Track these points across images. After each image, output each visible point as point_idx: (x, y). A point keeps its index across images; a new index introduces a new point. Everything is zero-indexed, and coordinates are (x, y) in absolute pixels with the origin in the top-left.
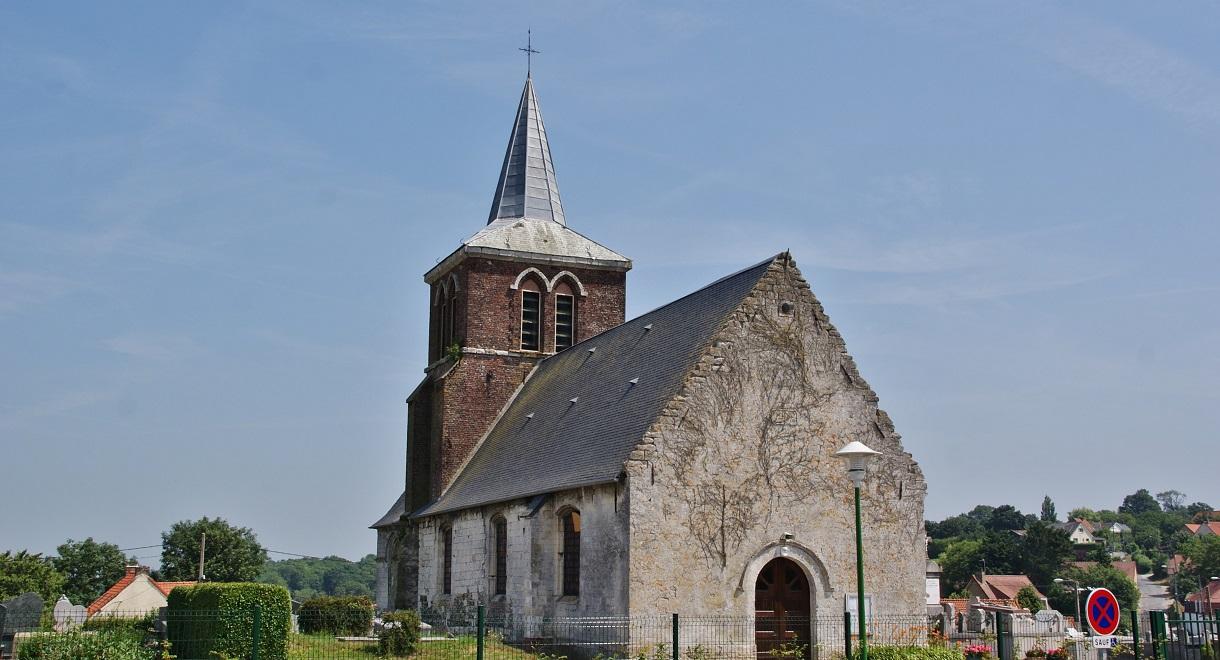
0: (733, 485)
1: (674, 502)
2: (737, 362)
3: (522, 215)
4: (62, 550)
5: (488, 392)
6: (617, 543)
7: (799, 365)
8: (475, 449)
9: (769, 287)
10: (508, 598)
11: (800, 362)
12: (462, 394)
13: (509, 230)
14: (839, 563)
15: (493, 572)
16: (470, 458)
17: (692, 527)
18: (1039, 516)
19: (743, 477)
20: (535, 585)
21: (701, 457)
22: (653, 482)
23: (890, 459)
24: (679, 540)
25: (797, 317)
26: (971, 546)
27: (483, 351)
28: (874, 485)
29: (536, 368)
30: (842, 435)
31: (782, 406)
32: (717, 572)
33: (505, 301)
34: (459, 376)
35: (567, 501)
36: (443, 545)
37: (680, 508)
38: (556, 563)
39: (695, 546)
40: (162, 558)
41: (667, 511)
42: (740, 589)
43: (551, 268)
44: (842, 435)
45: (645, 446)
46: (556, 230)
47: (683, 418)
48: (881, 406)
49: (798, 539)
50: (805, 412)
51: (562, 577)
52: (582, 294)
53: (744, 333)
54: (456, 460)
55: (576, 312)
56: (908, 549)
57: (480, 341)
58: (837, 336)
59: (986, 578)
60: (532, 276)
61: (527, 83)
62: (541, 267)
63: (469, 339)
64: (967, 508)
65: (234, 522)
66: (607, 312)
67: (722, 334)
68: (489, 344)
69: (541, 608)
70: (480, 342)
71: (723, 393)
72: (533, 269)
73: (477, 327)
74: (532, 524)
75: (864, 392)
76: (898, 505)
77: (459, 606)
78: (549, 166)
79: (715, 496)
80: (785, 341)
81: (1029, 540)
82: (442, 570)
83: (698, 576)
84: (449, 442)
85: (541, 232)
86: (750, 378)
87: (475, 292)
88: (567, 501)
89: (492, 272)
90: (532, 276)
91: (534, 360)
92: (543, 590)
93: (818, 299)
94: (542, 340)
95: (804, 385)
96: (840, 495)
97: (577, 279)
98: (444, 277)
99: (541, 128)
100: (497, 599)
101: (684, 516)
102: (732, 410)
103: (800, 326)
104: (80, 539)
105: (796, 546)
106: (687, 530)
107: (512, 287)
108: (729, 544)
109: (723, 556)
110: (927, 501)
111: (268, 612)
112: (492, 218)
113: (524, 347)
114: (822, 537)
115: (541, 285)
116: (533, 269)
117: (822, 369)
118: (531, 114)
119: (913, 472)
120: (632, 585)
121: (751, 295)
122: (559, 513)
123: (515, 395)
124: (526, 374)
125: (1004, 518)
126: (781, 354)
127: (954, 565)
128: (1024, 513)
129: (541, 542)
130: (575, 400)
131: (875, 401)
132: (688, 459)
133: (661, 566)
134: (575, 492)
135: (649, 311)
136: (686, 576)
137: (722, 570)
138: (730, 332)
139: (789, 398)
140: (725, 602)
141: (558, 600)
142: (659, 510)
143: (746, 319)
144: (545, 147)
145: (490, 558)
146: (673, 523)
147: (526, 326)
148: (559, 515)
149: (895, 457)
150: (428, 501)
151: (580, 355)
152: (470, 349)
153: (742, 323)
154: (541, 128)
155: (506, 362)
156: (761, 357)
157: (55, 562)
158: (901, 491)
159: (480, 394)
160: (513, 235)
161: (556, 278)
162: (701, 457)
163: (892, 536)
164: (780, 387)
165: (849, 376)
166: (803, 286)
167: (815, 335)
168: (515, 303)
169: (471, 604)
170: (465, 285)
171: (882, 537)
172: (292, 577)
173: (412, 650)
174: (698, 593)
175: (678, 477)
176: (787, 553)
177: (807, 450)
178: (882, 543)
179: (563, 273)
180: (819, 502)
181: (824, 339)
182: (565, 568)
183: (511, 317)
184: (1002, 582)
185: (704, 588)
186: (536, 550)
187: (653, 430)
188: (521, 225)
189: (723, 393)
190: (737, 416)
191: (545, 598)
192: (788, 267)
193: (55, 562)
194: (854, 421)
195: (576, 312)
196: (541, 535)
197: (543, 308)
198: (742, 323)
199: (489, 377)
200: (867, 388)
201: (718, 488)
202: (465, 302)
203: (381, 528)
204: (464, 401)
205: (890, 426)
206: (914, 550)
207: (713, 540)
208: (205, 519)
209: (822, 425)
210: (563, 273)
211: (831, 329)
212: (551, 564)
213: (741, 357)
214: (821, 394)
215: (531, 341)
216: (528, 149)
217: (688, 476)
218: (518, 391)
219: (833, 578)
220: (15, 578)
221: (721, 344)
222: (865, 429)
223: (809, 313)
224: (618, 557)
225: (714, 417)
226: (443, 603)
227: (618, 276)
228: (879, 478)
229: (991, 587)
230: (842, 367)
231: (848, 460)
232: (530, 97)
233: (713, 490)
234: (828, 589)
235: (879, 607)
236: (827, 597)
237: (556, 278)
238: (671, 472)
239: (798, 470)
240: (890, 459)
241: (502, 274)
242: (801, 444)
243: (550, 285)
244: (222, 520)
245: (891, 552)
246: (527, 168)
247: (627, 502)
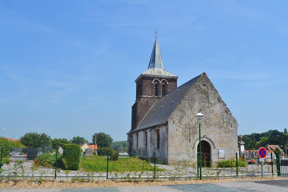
0: (192, 124)
1: (178, 128)
2: (193, 97)
3: (154, 67)
4: (74, 138)
5: (147, 105)
6: (166, 137)
8: (144, 117)
9: (200, 80)
10: (147, 149)
11: (208, 97)
13: (152, 71)
14: (217, 142)
15: (145, 143)
16: (143, 119)
17: (183, 134)
18: (283, 132)
19: (194, 122)
20: (151, 146)
21: (185, 118)
22: (174, 124)
23: (229, 118)
24: (180, 136)
26: (267, 139)
27: (146, 96)
28: (225, 124)
29: (157, 100)
30: (218, 113)
31: (204, 107)
32: (188, 143)
33: (150, 86)
34: (141, 102)
35: (157, 128)
36: (137, 137)
37: (180, 129)
38: (156, 141)
39: (183, 138)
40: (92, 140)
41: (177, 130)
42: (194, 147)
43: (160, 78)
44: (218, 113)
45: (172, 116)
46: (162, 70)
47: (181, 110)
49: (207, 136)
50: (209, 108)
51: (157, 145)
52: (167, 84)
53: (195, 91)
55: (166, 88)
56: (234, 139)
57: (145, 94)
58: (217, 91)
59: (269, 146)
60: (156, 80)
61: (156, 39)
62: (158, 78)
64: (267, 131)
65: (106, 133)
67: (189, 91)
68: (147, 95)
69: (152, 151)
71: (190, 104)
72: (156, 79)
73: (145, 91)
74: (151, 133)
75: (223, 103)
76: (231, 129)
77: (140, 151)
78: (160, 57)
79: (188, 127)
80: (204, 92)
81: (280, 137)
82: (137, 143)
83: (184, 144)
84: (139, 116)
85: (161, 71)
86: (196, 101)
88: (157, 128)
89: (148, 80)
90: (156, 80)
91: (157, 98)
92: (153, 147)
93: (212, 83)
94: (159, 94)
95: (209, 102)
96: (218, 127)
97: (166, 81)
98: (139, 81)
99: (159, 49)
100: (146, 149)
101: (181, 131)
102: (192, 108)
103: (208, 89)
104: (77, 136)
105: (207, 138)
106: (181, 134)
107: (152, 83)
109: (190, 140)
110: (238, 128)
111: (75, 151)
112: (148, 68)
113: (155, 95)
114: (212, 135)
116: (156, 79)
117: (213, 98)
118: (156, 46)
120: (169, 146)
121: (196, 82)
122: (156, 131)
123: (153, 106)
125: (275, 133)
126: (203, 95)
127: (262, 143)
128: (280, 132)
129: (152, 137)
130: (162, 106)
131: (226, 105)
132: (182, 118)
133: (175, 142)
134: (158, 126)
135: (180, 85)
136: (181, 144)
137: (190, 143)
138: (191, 90)
139: (205, 105)
140: (190, 150)
141: (156, 150)
142: (175, 131)
143: (195, 87)
144: (160, 53)
146: (178, 133)
147: (155, 91)
148: (156, 131)
149: (230, 118)
150: (135, 128)
151: (165, 97)
152: (143, 96)
153: (194, 88)
154: (159, 49)
155: (151, 99)
156: (199, 96)
157: (72, 140)
158: (232, 125)
159: (145, 106)
160: (152, 72)
161: (162, 81)
162: (185, 118)
163: (230, 136)
164: (203, 102)
165: (220, 100)
166: (208, 80)
167: (211, 91)
168: (153, 86)
169: (141, 150)
170: (142, 83)
171: (227, 136)
172: (124, 144)
173: (117, 159)
174: (184, 148)
175: (179, 122)
176: (205, 139)
177: (209, 116)
178: (227, 137)
179: (163, 79)
180: (212, 128)
181: (214, 91)
182: (157, 142)
184: (272, 147)
185: (185, 147)
186: (151, 138)
187: (174, 112)
188: (154, 69)
189: (190, 104)
190: (193, 109)
191: (153, 149)
192: (205, 76)
193: (72, 140)
194: (221, 110)
195: (166, 88)
196: (152, 135)
197: (159, 87)
199: (147, 102)
201: (189, 125)
202: (142, 86)
203: (128, 134)
204: (142, 107)
205: (229, 111)
206: (235, 139)
207: (187, 136)
208: (101, 132)
209: (213, 111)
210: (163, 79)
211: (215, 89)
212: (155, 141)
213: (194, 96)
214: (213, 104)
215: (156, 94)
216: (156, 53)
217: (182, 122)
218: (153, 105)
219: (216, 145)
220: (62, 143)
221: (189, 93)
222: (223, 112)
224: (166, 140)
226: (137, 150)
227: (175, 80)
228: (227, 123)
229: (270, 148)
231: (197, 117)
232: (156, 42)
233: (187, 125)
234: (214, 148)
235: (226, 152)
236: (214, 149)
237: (162, 81)
238: (178, 121)
239: (207, 121)
240: (229, 118)
242: (208, 115)
243: (160, 82)
244: (104, 133)
245: (229, 139)
246: (156, 57)
247: (168, 128)
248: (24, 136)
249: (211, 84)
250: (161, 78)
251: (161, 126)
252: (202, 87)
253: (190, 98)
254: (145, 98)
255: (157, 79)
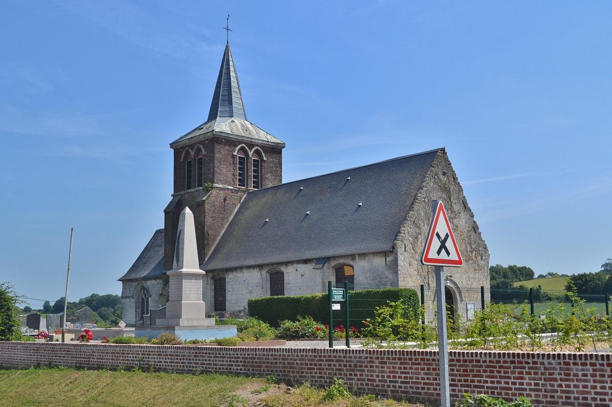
7: (450, 200)
11: (450, 198)
12: (213, 209)
17: (418, 272)
25: (448, 178)
27: (222, 186)
33: (231, 160)
34: (212, 199)
43: (251, 145)
48: (475, 219)
53: (432, 184)
54: (211, 243)
55: (261, 168)
57: (220, 181)
63: (215, 180)
66: (274, 169)
70: (220, 181)
72: (243, 145)
73: (219, 174)
87: (217, 155)
91: (244, 192)
97: (262, 151)
106: (417, 273)
107: (234, 154)
108: (430, 279)
115: (246, 154)
116: (243, 145)
117: (456, 201)
119: (485, 248)
124: (241, 199)
131: (473, 216)
145: (267, 291)
146: (412, 270)
152: (216, 185)
179: (256, 148)
181: (457, 188)
183: (234, 169)
194: (467, 225)
195: (261, 168)
197: (247, 166)
198: (431, 179)
199: (225, 200)
200: (470, 211)
205: (478, 228)
210: (256, 148)
223: (452, 176)
225: (423, 222)
230: (463, 201)
234: (462, 300)
241: (229, 146)
243: (251, 153)
248: (238, 272)
249: (454, 171)
250: (251, 144)
251: (359, 257)
252: (441, 177)
253: (426, 200)
254: (221, 189)
255: (243, 146)
